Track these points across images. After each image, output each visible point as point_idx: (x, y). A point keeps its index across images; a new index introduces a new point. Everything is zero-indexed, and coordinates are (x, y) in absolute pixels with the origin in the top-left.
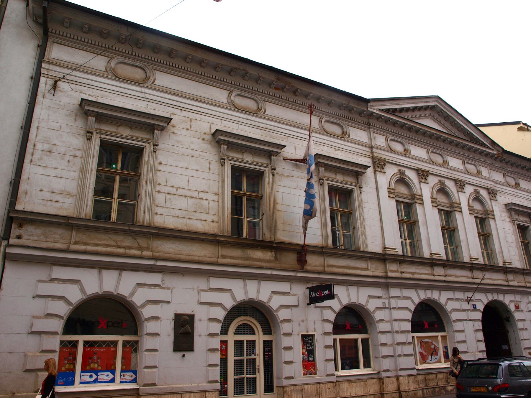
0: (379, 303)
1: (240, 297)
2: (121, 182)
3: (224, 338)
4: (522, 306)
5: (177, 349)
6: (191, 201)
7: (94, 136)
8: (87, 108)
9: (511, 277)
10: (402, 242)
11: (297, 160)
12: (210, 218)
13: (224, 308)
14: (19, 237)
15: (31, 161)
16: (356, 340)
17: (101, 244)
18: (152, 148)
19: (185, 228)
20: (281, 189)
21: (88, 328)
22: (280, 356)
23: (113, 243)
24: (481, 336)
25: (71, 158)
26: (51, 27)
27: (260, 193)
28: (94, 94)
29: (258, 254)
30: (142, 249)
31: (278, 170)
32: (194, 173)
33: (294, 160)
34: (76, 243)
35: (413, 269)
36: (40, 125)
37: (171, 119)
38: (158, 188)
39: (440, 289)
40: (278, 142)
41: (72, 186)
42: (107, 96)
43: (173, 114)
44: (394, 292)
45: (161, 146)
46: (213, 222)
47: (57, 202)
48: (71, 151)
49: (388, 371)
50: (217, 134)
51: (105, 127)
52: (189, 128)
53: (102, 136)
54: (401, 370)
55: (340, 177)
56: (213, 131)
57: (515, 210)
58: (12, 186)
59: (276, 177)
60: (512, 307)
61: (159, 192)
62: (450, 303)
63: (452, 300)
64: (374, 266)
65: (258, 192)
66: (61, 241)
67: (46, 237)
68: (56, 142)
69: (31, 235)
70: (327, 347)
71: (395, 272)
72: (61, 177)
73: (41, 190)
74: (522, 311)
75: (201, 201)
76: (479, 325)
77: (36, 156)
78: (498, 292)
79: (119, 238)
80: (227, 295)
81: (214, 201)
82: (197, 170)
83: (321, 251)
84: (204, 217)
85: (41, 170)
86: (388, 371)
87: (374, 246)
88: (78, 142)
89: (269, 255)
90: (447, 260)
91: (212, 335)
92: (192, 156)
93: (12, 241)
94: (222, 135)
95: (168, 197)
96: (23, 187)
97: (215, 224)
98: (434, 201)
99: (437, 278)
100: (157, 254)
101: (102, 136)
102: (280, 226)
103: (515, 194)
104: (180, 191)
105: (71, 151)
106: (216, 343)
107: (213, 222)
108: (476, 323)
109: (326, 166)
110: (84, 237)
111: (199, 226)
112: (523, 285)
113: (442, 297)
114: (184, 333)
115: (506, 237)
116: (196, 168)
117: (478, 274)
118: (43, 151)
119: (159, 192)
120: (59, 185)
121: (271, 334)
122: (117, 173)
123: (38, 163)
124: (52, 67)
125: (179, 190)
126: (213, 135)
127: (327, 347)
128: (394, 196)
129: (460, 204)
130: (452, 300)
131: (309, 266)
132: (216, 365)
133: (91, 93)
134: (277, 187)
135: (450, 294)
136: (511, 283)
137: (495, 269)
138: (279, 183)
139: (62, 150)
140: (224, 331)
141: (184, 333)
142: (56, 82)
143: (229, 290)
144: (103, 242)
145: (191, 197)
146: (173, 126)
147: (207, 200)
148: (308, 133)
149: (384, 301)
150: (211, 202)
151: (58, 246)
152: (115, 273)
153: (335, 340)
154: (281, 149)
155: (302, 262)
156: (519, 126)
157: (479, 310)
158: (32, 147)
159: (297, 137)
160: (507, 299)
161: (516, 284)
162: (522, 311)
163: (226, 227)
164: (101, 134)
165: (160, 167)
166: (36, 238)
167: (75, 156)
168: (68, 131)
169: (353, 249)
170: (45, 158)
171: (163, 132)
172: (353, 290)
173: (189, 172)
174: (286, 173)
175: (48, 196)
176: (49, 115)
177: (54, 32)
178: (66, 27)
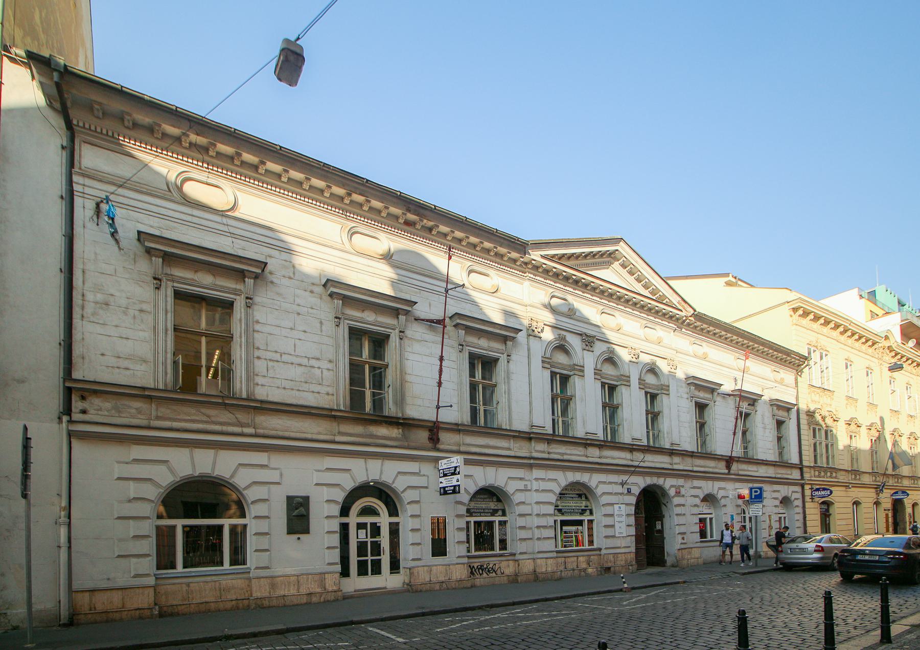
0: (520, 485)
1: (361, 478)
2: (207, 343)
3: (345, 520)
4: (683, 491)
5: (291, 531)
6: (300, 370)
7: (163, 284)
8: (148, 244)
9: (677, 459)
10: (553, 420)
11: (432, 321)
12: (324, 390)
13: (343, 489)
14: (84, 412)
15: (83, 316)
16: (174, 527)
17: (188, 418)
18: (243, 303)
19: (294, 402)
20: (411, 357)
21: (190, 511)
22: (406, 538)
23: (205, 418)
24: (632, 520)
25: (137, 313)
26: (77, 117)
27: (494, 380)
28: (156, 225)
29: (383, 431)
30: (242, 425)
31: (409, 333)
32: (302, 335)
33: (427, 321)
34: (158, 418)
35: (562, 449)
36: (87, 267)
37: (266, 264)
38: (257, 353)
39: (666, 476)
40: (407, 297)
41: (145, 350)
42: (175, 228)
43: (270, 257)
44: (537, 473)
45: (513, 357)
46: (328, 394)
47: (127, 369)
48: (134, 303)
49: (525, 553)
50: (329, 285)
51: (178, 272)
52: (292, 276)
53: (175, 285)
54: (539, 552)
55: (483, 342)
56: (324, 281)
57: (696, 385)
58: (62, 349)
59: (406, 341)
60: (672, 492)
61: (259, 358)
62: (601, 486)
63: (604, 483)
64: (517, 445)
65: (491, 379)
66: (139, 416)
67: (120, 412)
68: (112, 291)
69: (99, 410)
70: (459, 529)
71: (543, 452)
72: (128, 337)
73: (103, 355)
74: (683, 496)
75: (313, 370)
76: (632, 510)
77: (89, 309)
78: (659, 475)
79: (212, 412)
80: (347, 475)
81: (328, 370)
82: (305, 332)
83: (456, 428)
84: (317, 388)
85: (99, 329)
86: (525, 553)
87: (520, 424)
88: (145, 292)
89: (395, 432)
90: (648, 446)
91: (458, 516)
92: (299, 314)
93: (76, 416)
94: (335, 287)
95: (270, 364)
96: (77, 351)
97: (330, 397)
98: (597, 372)
99: (590, 460)
100: (261, 431)
101: (175, 285)
102: (409, 400)
103: (189, 218)
104: (285, 358)
105: (134, 303)
106: (335, 525)
107: (328, 394)
108: (629, 507)
109: (468, 329)
110: (168, 411)
111: (309, 400)
112: (691, 468)
113: (592, 480)
114: (298, 516)
115: (679, 416)
116: (304, 329)
117: (639, 456)
118: (96, 303)
119: (259, 358)
120: (126, 348)
121: (397, 515)
122: (201, 334)
123: (92, 319)
124: (88, 182)
125: (284, 356)
126: (325, 285)
127: (459, 529)
128: (549, 366)
129: (629, 377)
130: (604, 483)
131: (443, 444)
132: (336, 547)
133: (152, 223)
134: (406, 354)
135: (602, 477)
136: (676, 467)
137: (660, 451)
138: (409, 349)
139: (124, 302)
140: (345, 512)
141: (298, 516)
142: (98, 205)
143: (166, 462)
144: (193, 418)
145: (300, 365)
146: (271, 273)
147: (319, 368)
148: (444, 285)
149: (526, 483)
150: (325, 372)
151: (135, 422)
152: (211, 452)
153: (468, 523)
154: (412, 306)
155: (434, 440)
156: (726, 279)
157: (634, 494)
158: (80, 297)
159: (432, 292)
160: (668, 483)
161: (681, 467)
162: (683, 496)
163: (466, 418)
164: (173, 281)
165: (257, 327)
166: (106, 413)
167: (141, 311)
168: (127, 276)
169: (495, 426)
170: (101, 312)
171: (258, 281)
172: (490, 471)
173: (295, 334)
174: (417, 336)
175: (113, 361)
176: (96, 254)
177: (81, 124)
178: (98, 117)
